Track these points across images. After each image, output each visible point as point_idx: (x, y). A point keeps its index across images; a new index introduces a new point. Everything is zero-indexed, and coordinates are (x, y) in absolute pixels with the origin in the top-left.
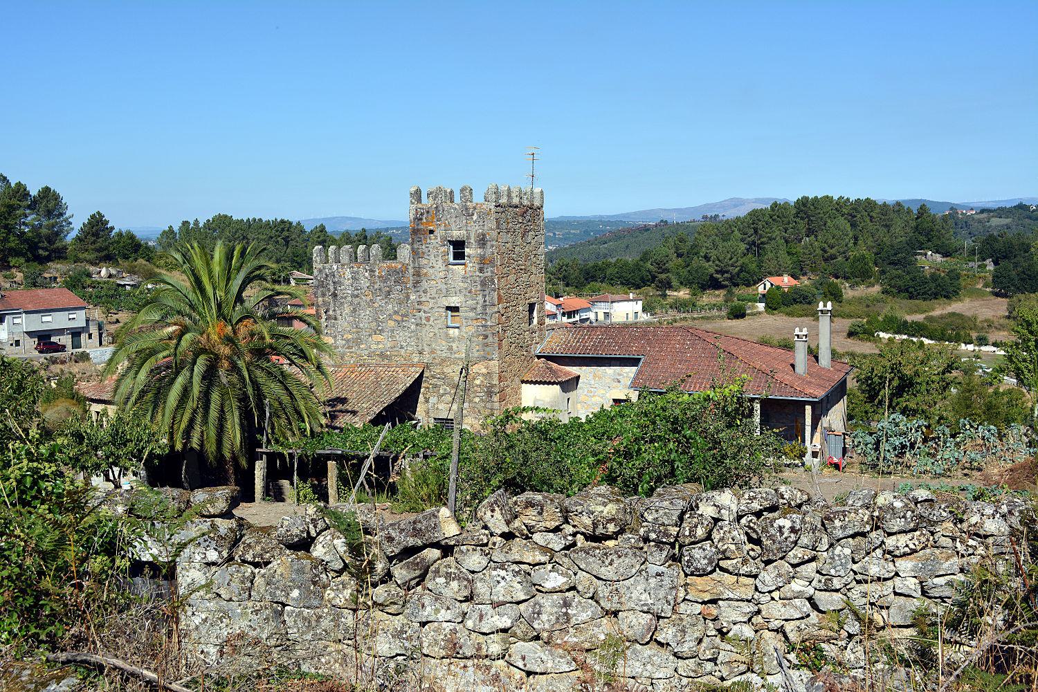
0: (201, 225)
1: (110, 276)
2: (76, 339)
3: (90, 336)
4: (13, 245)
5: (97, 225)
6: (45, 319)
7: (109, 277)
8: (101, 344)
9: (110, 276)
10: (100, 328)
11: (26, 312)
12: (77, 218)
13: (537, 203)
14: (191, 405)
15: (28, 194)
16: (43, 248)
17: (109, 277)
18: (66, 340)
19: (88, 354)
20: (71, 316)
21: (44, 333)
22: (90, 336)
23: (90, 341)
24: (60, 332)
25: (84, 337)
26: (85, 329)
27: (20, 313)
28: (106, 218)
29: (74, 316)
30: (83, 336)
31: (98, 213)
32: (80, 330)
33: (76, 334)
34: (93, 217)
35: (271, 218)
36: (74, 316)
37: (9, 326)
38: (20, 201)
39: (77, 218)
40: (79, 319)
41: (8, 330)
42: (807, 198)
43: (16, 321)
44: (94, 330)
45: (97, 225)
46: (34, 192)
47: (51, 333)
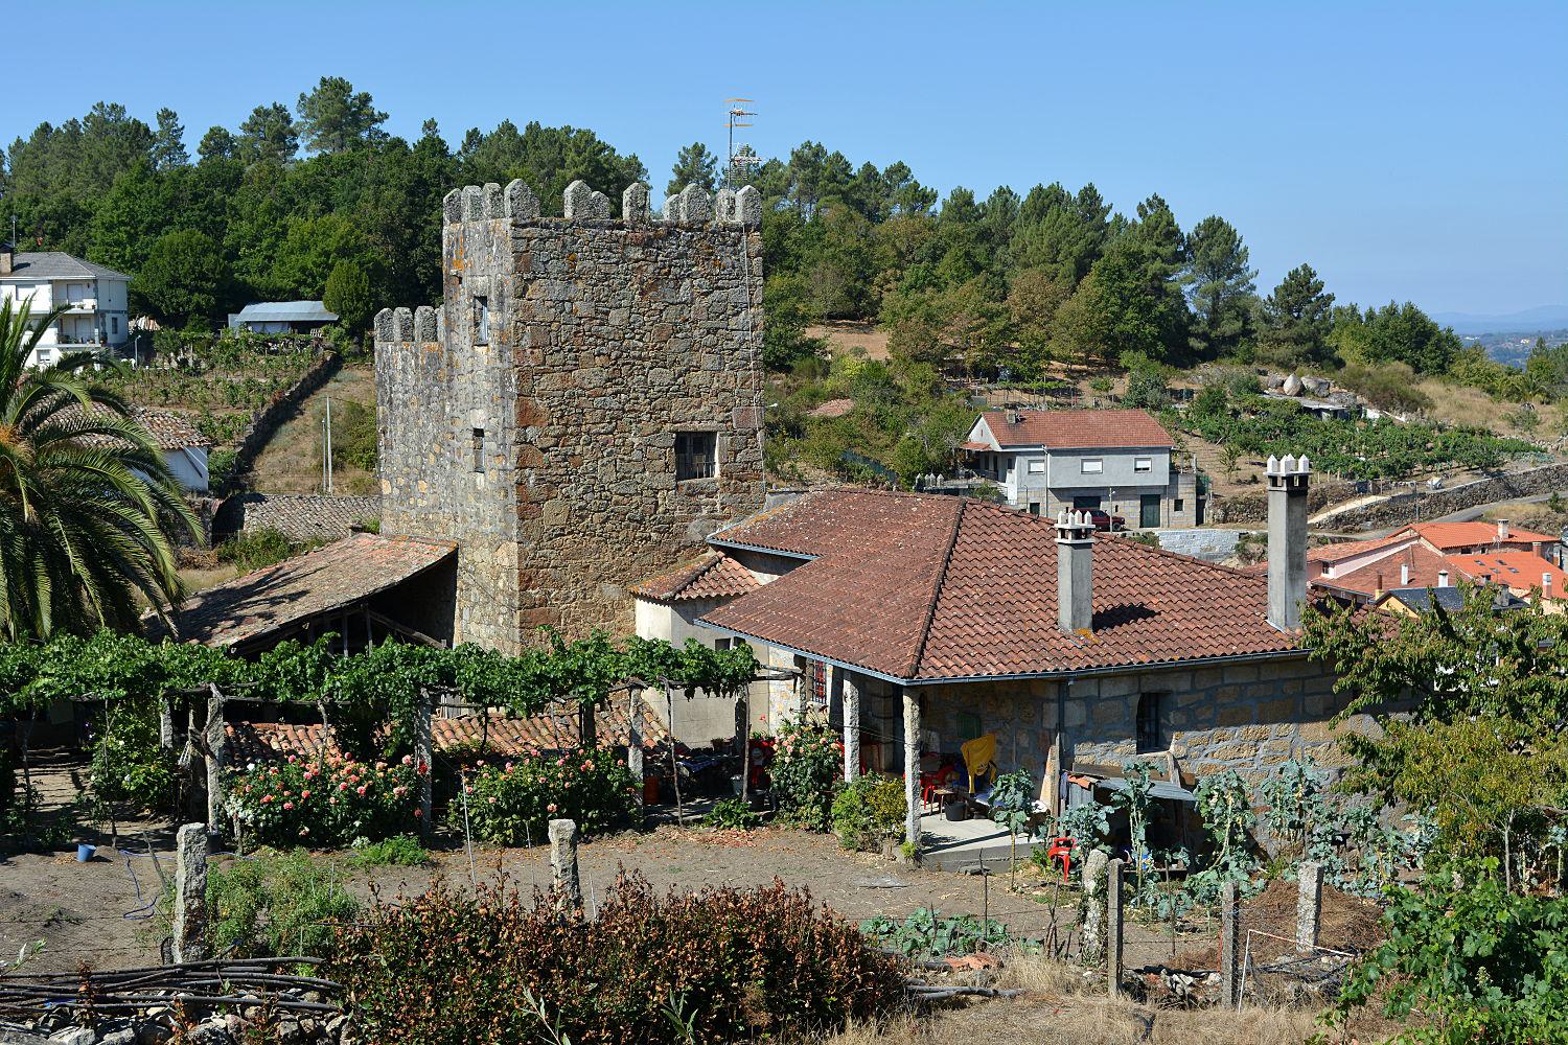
0: (1333, 304)
1: (1302, 391)
2: (1149, 508)
3: (1178, 505)
4: (1129, 327)
5: (1302, 289)
6: (1088, 467)
7: (1299, 394)
8: (1199, 521)
9: (1302, 391)
10: (1200, 490)
11: (1054, 452)
12: (1266, 279)
13: (1458, 368)
14: (52, 994)
15: (1177, 232)
16: (1197, 336)
17: (1299, 394)
18: (1130, 510)
19: (1156, 538)
20: (1140, 465)
21: (1086, 494)
22: (1178, 505)
23: (1178, 513)
24: (1123, 492)
25: (1166, 505)
26: (1170, 489)
27: (1043, 453)
28: (1319, 277)
29: (1147, 464)
30: (1163, 503)
31: (1305, 267)
32: (1156, 492)
33: (1149, 499)
34: (1294, 275)
35: (1379, 304)
36: (1147, 464)
37: (1020, 477)
38: (1159, 244)
39: (1266, 279)
40: (1155, 473)
41: (1019, 483)
42: (819, 152)
43: (1035, 467)
44: (1187, 493)
45: (1302, 289)
46: (1187, 225)
47: (1100, 493)
